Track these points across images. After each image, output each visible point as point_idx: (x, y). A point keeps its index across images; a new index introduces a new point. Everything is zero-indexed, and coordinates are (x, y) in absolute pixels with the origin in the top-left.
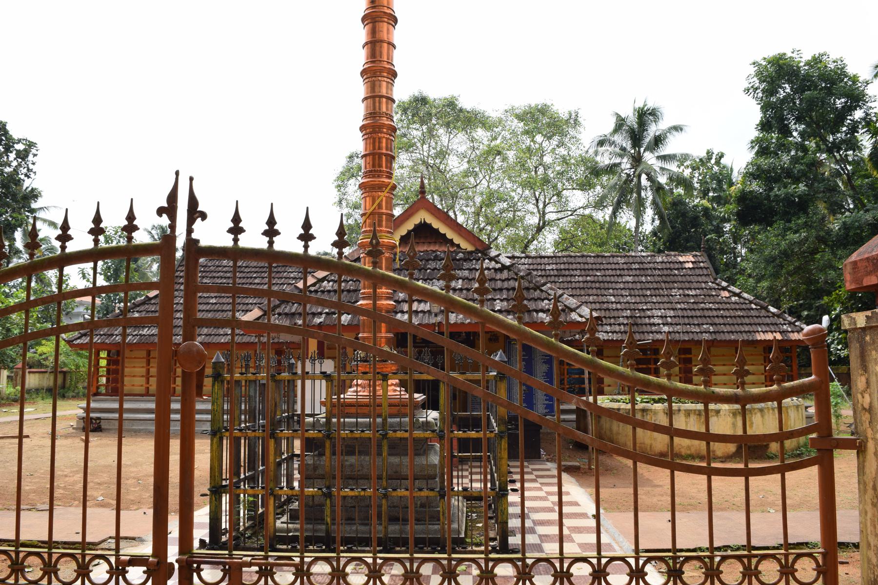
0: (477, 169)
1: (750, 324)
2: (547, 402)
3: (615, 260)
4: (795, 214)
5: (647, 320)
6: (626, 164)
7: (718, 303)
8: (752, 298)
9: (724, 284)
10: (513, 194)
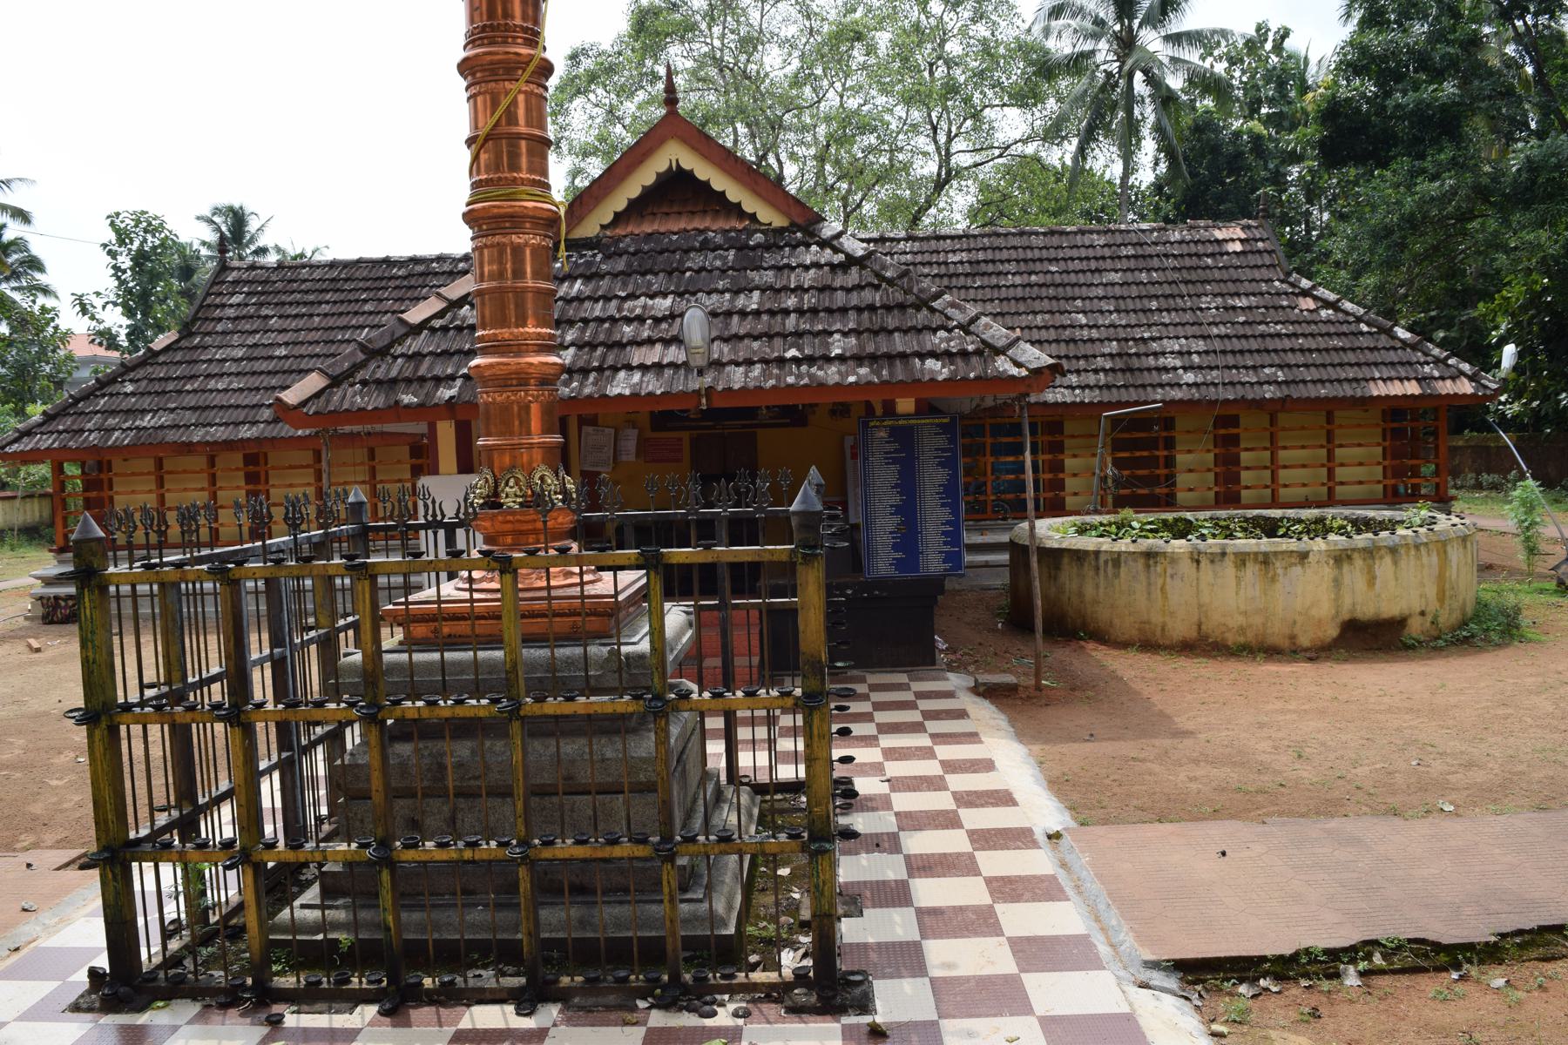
0: (819, 71)
1: (1358, 365)
2: (947, 548)
3: (1087, 240)
4: (1435, 141)
5: (1151, 361)
6: (1104, 53)
7: (1293, 323)
10: (887, 117)
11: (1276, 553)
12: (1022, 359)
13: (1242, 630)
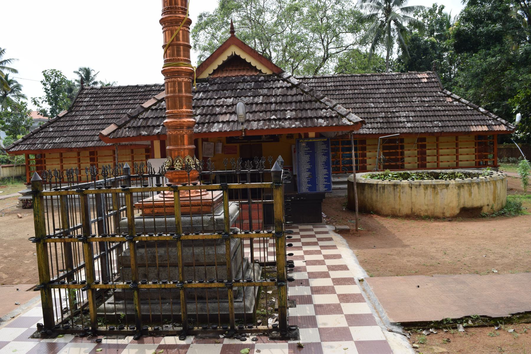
0: (283, 21)
1: (467, 120)
2: (326, 183)
3: (374, 78)
4: (493, 44)
5: (396, 119)
6: (380, 14)
8: (468, 102)
9: (449, 93)
10: (307, 36)
11: (438, 185)
12: (351, 119)
13: (426, 211)
